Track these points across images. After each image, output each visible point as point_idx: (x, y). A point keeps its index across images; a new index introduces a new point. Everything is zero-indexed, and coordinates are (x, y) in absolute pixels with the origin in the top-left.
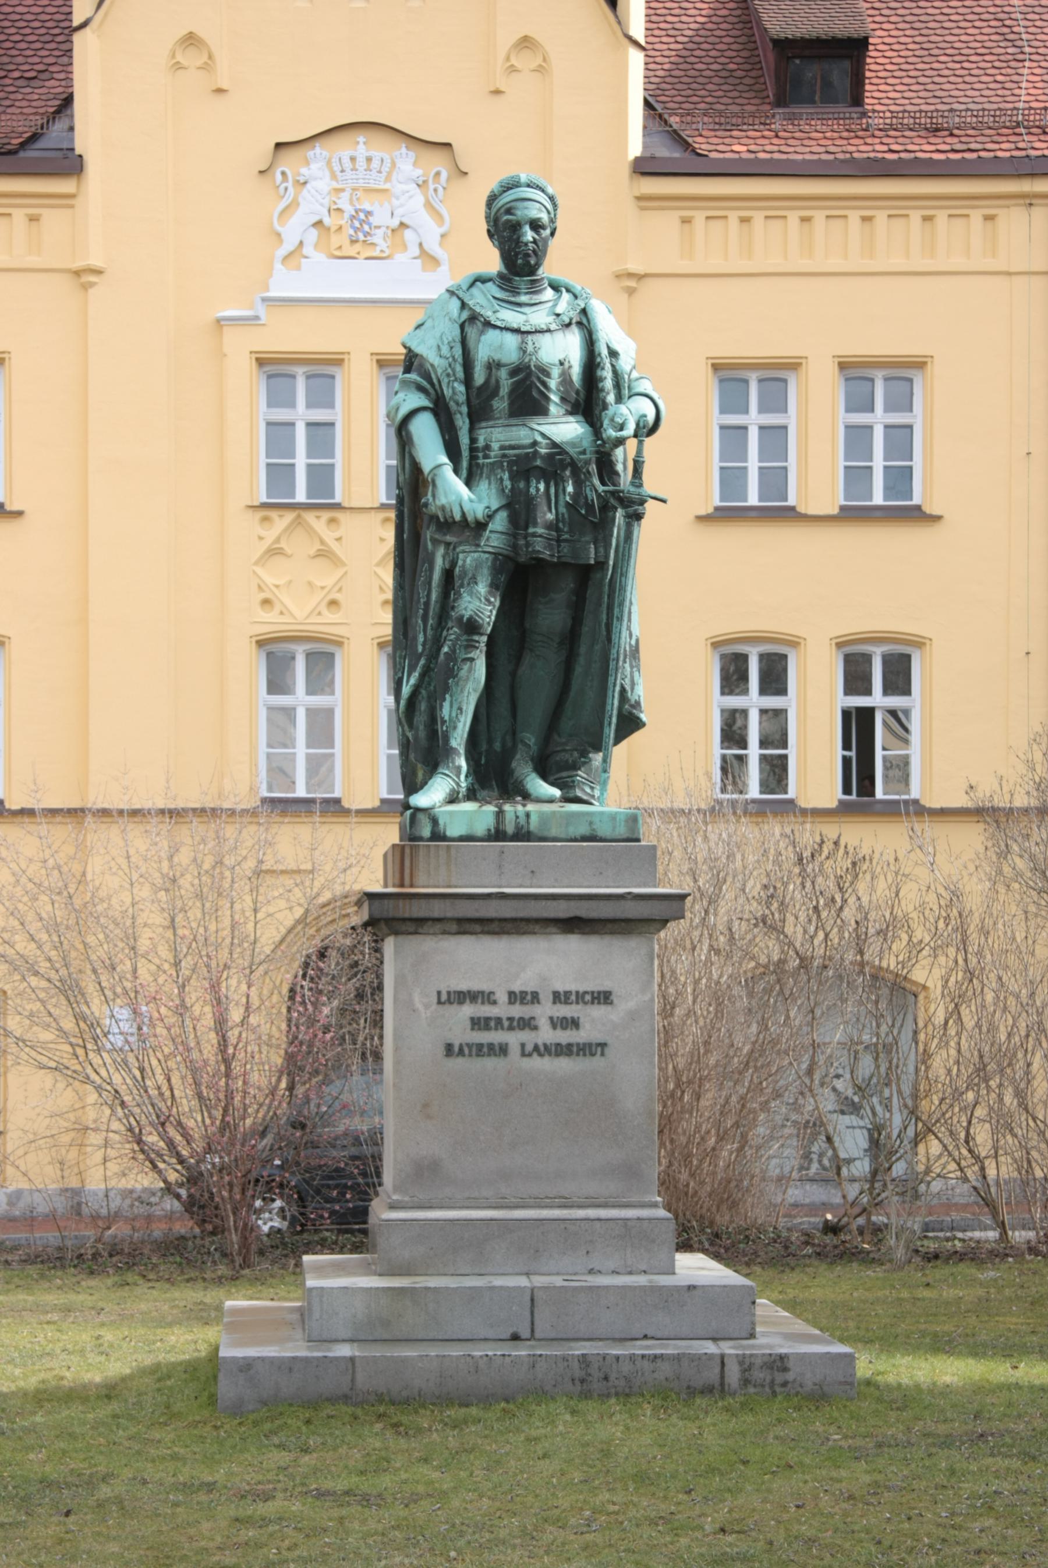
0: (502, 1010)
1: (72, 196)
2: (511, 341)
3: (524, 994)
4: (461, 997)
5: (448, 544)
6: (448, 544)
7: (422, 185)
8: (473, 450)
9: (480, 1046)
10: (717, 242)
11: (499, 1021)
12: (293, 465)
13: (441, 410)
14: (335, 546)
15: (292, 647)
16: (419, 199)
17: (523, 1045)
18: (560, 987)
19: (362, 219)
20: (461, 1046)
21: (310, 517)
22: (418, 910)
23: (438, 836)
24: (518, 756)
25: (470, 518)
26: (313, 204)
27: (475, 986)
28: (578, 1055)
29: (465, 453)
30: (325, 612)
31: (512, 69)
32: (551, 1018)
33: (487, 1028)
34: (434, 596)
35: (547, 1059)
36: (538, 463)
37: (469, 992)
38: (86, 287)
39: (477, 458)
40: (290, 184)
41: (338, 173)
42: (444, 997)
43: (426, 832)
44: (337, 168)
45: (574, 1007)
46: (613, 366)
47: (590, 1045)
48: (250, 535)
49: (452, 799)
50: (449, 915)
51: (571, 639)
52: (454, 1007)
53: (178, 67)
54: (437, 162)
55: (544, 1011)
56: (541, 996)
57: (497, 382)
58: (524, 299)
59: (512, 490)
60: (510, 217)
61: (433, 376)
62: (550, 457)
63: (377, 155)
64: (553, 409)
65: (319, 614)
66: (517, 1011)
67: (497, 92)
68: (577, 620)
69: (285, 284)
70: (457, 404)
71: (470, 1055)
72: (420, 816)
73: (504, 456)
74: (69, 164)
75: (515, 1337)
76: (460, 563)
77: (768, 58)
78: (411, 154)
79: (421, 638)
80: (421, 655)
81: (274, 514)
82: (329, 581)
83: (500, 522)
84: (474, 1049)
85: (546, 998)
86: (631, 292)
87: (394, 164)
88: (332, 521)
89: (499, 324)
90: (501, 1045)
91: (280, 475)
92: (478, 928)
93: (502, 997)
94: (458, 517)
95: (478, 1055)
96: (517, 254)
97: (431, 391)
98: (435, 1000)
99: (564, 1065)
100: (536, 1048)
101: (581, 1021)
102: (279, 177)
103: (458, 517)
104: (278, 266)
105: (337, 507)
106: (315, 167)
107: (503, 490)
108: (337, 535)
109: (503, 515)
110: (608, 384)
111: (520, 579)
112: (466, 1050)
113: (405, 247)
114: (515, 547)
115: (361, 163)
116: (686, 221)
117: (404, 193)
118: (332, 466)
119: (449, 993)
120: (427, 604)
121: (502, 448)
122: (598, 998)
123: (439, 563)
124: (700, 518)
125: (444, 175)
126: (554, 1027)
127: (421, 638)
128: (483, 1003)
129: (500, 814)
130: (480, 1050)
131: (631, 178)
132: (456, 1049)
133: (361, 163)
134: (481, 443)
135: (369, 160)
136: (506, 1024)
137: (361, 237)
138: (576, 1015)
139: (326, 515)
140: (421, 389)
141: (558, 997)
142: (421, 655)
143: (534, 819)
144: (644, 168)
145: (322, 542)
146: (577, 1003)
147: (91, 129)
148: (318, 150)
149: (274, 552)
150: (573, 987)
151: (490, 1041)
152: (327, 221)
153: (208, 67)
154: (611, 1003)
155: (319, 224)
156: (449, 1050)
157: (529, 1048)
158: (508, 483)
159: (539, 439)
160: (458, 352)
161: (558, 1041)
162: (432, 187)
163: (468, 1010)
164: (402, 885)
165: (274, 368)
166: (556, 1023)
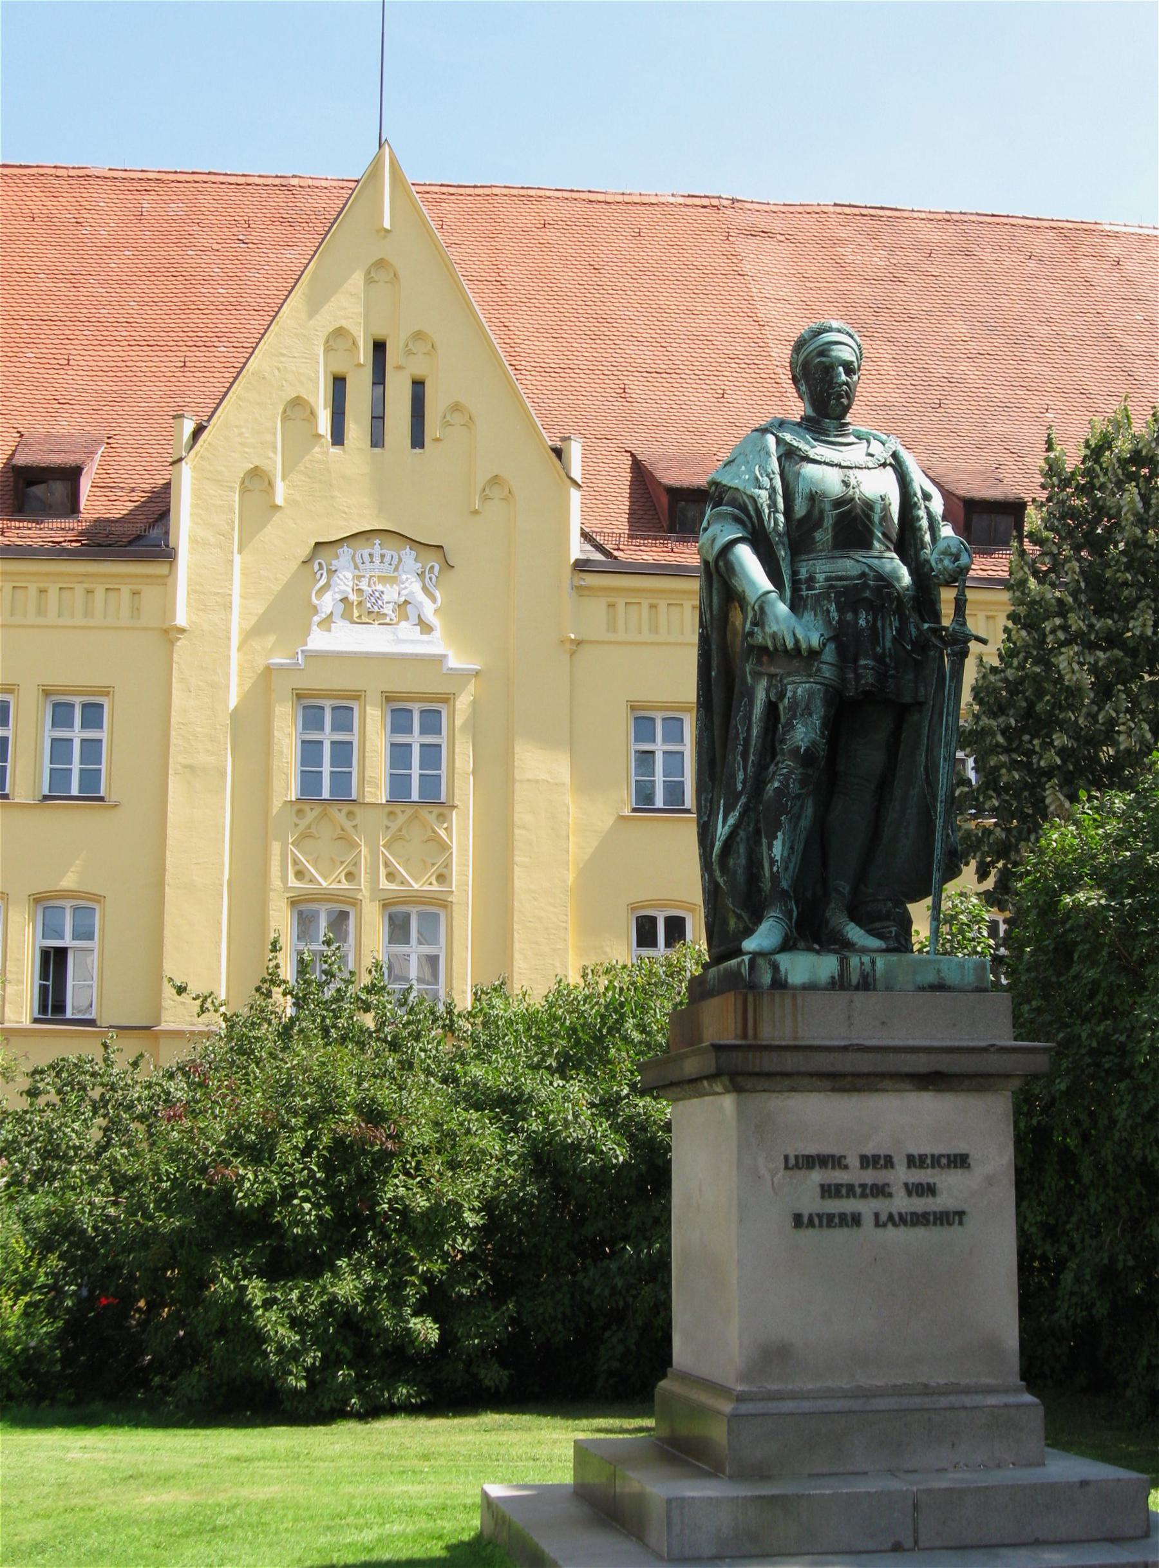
0: (855, 1175)
4: (810, 1162)
5: (771, 676)
6: (771, 676)
7: (421, 575)
9: (830, 1217)
11: (850, 1188)
12: (321, 772)
15: (313, 906)
18: (915, 1151)
20: (811, 1216)
22: (770, 1062)
23: (779, 984)
24: (832, 905)
25: (804, 646)
26: (344, 582)
27: (826, 1150)
28: (935, 1224)
32: (906, 1185)
34: (755, 732)
35: (902, 1228)
36: (867, 594)
37: (818, 1156)
39: (801, 590)
41: (360, 565)
42: (792, 1162)
43: (767, 979)
44: (359, 561)
45: (929, 1171)
46: (926, 507)
47: (947, 1213)
49: (787, 946)
50: (803, 1069)
51: (884, 785)
52: (801, 1174)
55: (901, 1175)
56: (895, 1160)
57: (822, 512)
59: (840, 621)
60: (823, 359)
61: (750, 508)
62: (879, 589)
65: (339, 882)
66: (870, 1177)
71: (821, 1226)
72: (760, 961)
73: (832, 586)
75: (897, 1548)
76: (789, 694)
78: (414, 553)
79: (740, 776)
80: (741, 793)
83: (829, 654)
84: (825, 1221)
87: (400, 559)
89: (818, 458)
90: (853, 1215)
93: (853, 1161)
94: (790, 645)
95: (829, 1226)
96: (829, 395)
97: (749, 525)
98: (783, 1166)
99: (920, 1234)
100: (891, 1217)
101: (939, 1185)
102: (316, 567)
103: (790, 645)
104: (315, 628)
107: (830, 622)
108: (354, 823)
109: (831, 648)
110: (924, 523)
111: (843, 712)
112: (816, 1221)
114: (843, 680)
115: (377, 560)
116: (611, 606)
119: (797, 1157)
120: (747, 740)
121: (827, 579)
122: (955, 1162)
123: (760, 696)
125: (437, 568)
126: (909, 1193)
127: (740, 776)
128: (833, 1168)
131: (573, 574)
132: (806, 1220)
133: (377, 560)
134: (803, 574)
135: (382, 556)
136: (858, 1191)
137: (376, 609)
138: (931, 1181)
140: (737, 520)
141: (913, 1161)
142: (741, 793)
146: (933, 1167)
151: (842, 1210)
154: (969, 1167)
156: (798, 1220)
157: (883, 1218)
158: (835, 615)
159: (867, 570)
161: (913, 1210)
162: (428, 576)
163: (817, 1177)
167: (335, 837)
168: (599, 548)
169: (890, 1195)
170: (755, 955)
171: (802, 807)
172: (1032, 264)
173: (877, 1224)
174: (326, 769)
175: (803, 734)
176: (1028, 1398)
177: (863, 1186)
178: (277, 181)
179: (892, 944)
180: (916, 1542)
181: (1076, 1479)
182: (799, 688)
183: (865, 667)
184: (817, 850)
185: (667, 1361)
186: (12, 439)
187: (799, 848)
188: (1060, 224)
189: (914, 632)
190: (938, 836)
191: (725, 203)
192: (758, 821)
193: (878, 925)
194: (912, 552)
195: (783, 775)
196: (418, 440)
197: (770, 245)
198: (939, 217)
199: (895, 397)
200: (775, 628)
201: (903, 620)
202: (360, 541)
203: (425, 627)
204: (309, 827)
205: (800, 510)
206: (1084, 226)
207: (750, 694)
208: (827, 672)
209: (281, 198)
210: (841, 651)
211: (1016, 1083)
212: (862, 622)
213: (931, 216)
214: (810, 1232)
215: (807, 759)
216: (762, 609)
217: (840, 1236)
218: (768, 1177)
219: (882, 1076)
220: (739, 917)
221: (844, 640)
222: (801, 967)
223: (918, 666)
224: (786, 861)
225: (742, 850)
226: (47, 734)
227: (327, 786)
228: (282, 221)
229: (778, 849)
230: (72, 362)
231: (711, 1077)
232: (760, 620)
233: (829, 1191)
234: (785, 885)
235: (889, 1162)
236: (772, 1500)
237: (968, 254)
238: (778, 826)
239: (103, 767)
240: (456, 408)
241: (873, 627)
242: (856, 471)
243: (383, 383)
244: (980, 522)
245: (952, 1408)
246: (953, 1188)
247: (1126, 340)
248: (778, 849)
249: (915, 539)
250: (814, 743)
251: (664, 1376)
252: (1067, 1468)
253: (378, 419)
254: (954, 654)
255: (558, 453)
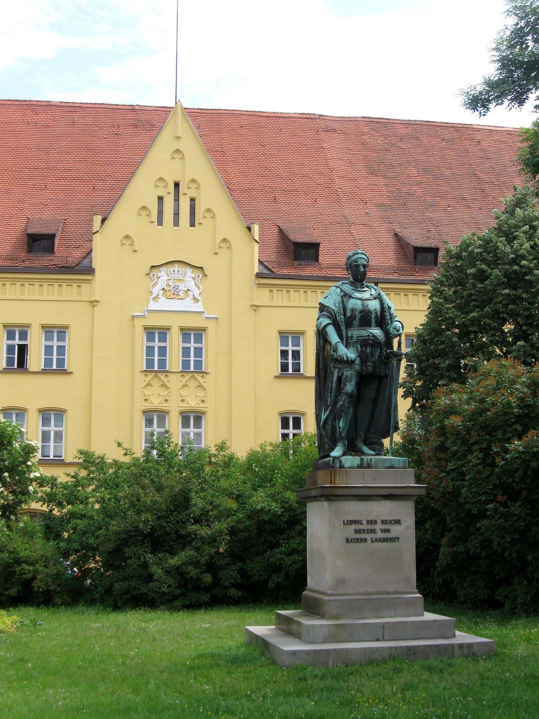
0: (365, 526)
1: (91, 280)
2: (359, 302)
3: (372, 521)
4: (351, 522)
5: (339, 368)
6: (339, 368)
8: (347, 337)
10: (280, 297)
11: (364, 530)
13: (336, 324)
14: (167, 383)
16: (193, 283)
17: (372, 539)
18: (384, 519)
19: (176, 288)
21: (159, 374)
22: (339, 492)
23: (342, 467)
26: (162, 283)
29: (345, 338)
30: (164, 403)
31: (220, 247)
33: (360, 533)
38: (94, 306)
40: (155, 278)
42: (346, 522)
44: (169, 273)
45: (388, 525)
48: (141, 380)
49: (344, 454)
50: (349, 494)
51: (375, 402)
53: (123, 244)
54: (199, 273)
55: (379, 526)
57: (355, 315)
58: (359, 289)
59: (361, 351)
63: (181, 270)
64: (373, 325)
66: (370, 527)
67: (216, 253)
68: (378, 394)
69: (153, 306)
70: (342, 322)
72: (336, 460)
73: (359, 339)
74: (90, 271)
76: (345, 374)
77: (292, 247)
79: (329, 400)
80: (329, 406)
81: (148, 374)
82: (165, 394)
83: (358, 362)
85: (379, 522)
86: (255, 310)
87: (186, 273)
88: (166, 376)
91: (150, 363)
92: (357, 498)
93: (365, 522)
94: (345, 359)
95: (357, 542)
100: (376, 539)
102: (152, 276)
103: (345, 359)
104: (151, 301)
105: (168, 372)
106: (163, 273)
109: (358, 359)
111: (363, 380)
113: (189, 296)
114: (362, 369)
115: (176, 271)
117: (189, 281)
118: (166, 359)
120: (331, 388)
121: (357, 337)
124: (276, 377)
125: (201, 276)
126: (382, 532)
127: (329, 400)
129: (362, 460)
130: (357, 540)
133: (176, 271)
134: (350, 335)
135: (179, 271)
136: (366, 531)
137: (176, 293)
139: (164, 374)
140: (328, 317)
141: (384, 522)
143: (373, 460)
144: (259, 276)
145: (163, 382)
147: (98, 260)
148: (163, 268)
149: (148, 385)
150: (388, 518)
152: (166, 288)
153: (132, 244)
155: (163, 289)
156: (347, 540)
157: (374, 539)
160: (341, 305)
163: (353, 527)
164: (331, 484)
165: (150, 332)
166: (383, 531)
167: (160, 385)
168: (266, 267)
169: (376, 533)
170: (335, 458)
171: (349, 410)
172: (444, 143)
173: (372, 542)
174: (156, 358)
175: (350, 387)
176: (419, 595)
177: (368, 530)
178: (130, 108)
179: (377, 452)
180: (383, 638)
181: (433, 619)
182: (348, 373)
183: (369, 365)
184: (354, 422)
185: (306, 585)
186: (25, 221)
187: (348, 423)
188: (456, 125)
189: (385, 353)
190: (392, 419)
191: (316, 117)
192: (335, 414)
193: (373, 446)
194: (384, 326)
195: (342, 401)
196: (192, 224)
197: (335, 135)
198: (405, 122)
199: (386, 201)
200: (341, 354)
201: (381, 349)
202: (170, 266)
203: (196, 300)
204: (150, 381)
205: (349, 314)
206: (466, 126)
207: (333, 374)
208: (357, 367)
209: (131, 115)
210: (362, 360)
211: (415, 498)
212: (368, 351)
213: (402, 122)
214: (351, 544)
215: (350, 396)
216: (336, 347)
217: (362, 545)
218: (338, 526)
219: (374, 496)
220: (329, 444)
221: (362, 356)
222: (350, 461)
223: (386, 364)
224: (344, 428)
225: (330, 423)
226: (43, 344)
227: (155, 366)
228: (133, 125)
229: (341, 424)
230: (47, 187)
231: (321, 496)
232: (335, 350)
233: (357, 531)
234: (343, 435)
235: (376, 522)
236: (340, 625)
237: (417, 139)
238: (341, 417)
239: (66, 357)
240: (209, 210)
241: (372, 353)
242: (367, 301)
243: (178, 200)
244: (420, 256)
245: (395, 598)
246: (395, 531)
247: (482, 176)
248: (341, 424)
249: (385, 322)
250: (353, 390)
251: (304, 590)
252: (429, 616)
253: (176, 214)
254: (397, 360)
255: (249, 229)
